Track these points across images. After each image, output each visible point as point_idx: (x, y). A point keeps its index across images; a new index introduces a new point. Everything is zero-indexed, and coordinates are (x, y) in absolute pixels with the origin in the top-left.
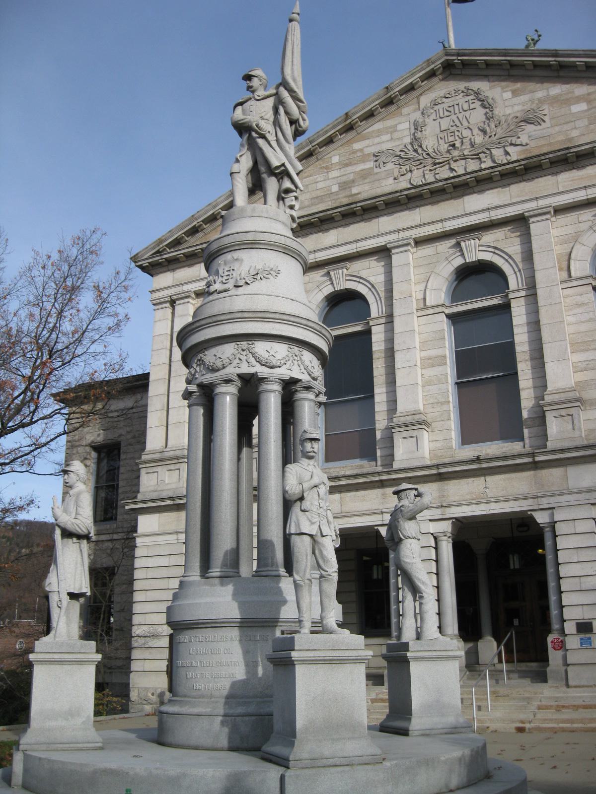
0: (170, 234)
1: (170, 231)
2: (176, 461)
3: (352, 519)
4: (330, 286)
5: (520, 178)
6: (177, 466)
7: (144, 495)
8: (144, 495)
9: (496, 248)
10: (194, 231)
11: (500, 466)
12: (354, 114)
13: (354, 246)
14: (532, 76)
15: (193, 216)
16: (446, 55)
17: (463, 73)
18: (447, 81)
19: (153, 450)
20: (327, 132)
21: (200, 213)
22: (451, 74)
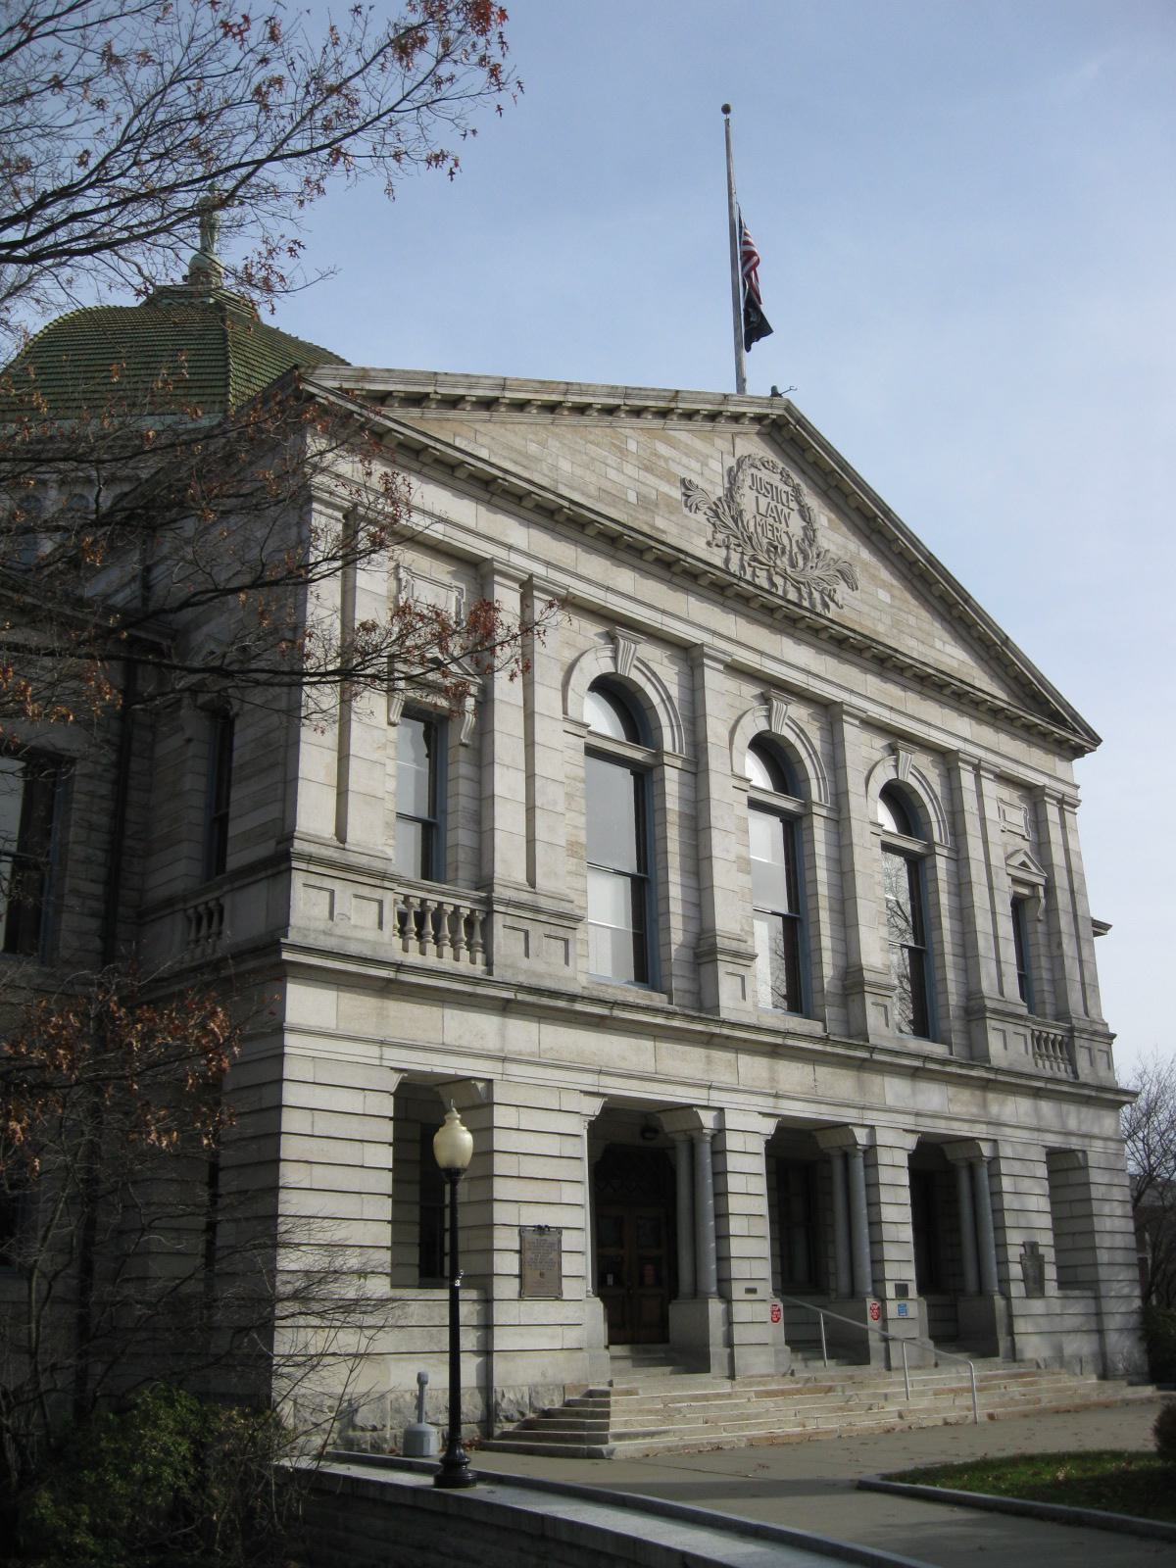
0: (386, 374)
1: (388, 370)
2: (378, 882)
3: (670, 1088)
4: (609, 662)
5: (721, 599)
6: (378, 894)
7: (306, 936)
8: (306, 936)
9: (802, 730)
10: (417, 400)
11: (448, 990)
12: (684, 400)
13: (658, 617)
14: (845, 514)
15: (436, 374)
16: (786, 409)
17: (783, 446)
18: (763, 440)
19: (316, 836)
20: (647, 397)
21: (448, 378)
22: (769, 434)
